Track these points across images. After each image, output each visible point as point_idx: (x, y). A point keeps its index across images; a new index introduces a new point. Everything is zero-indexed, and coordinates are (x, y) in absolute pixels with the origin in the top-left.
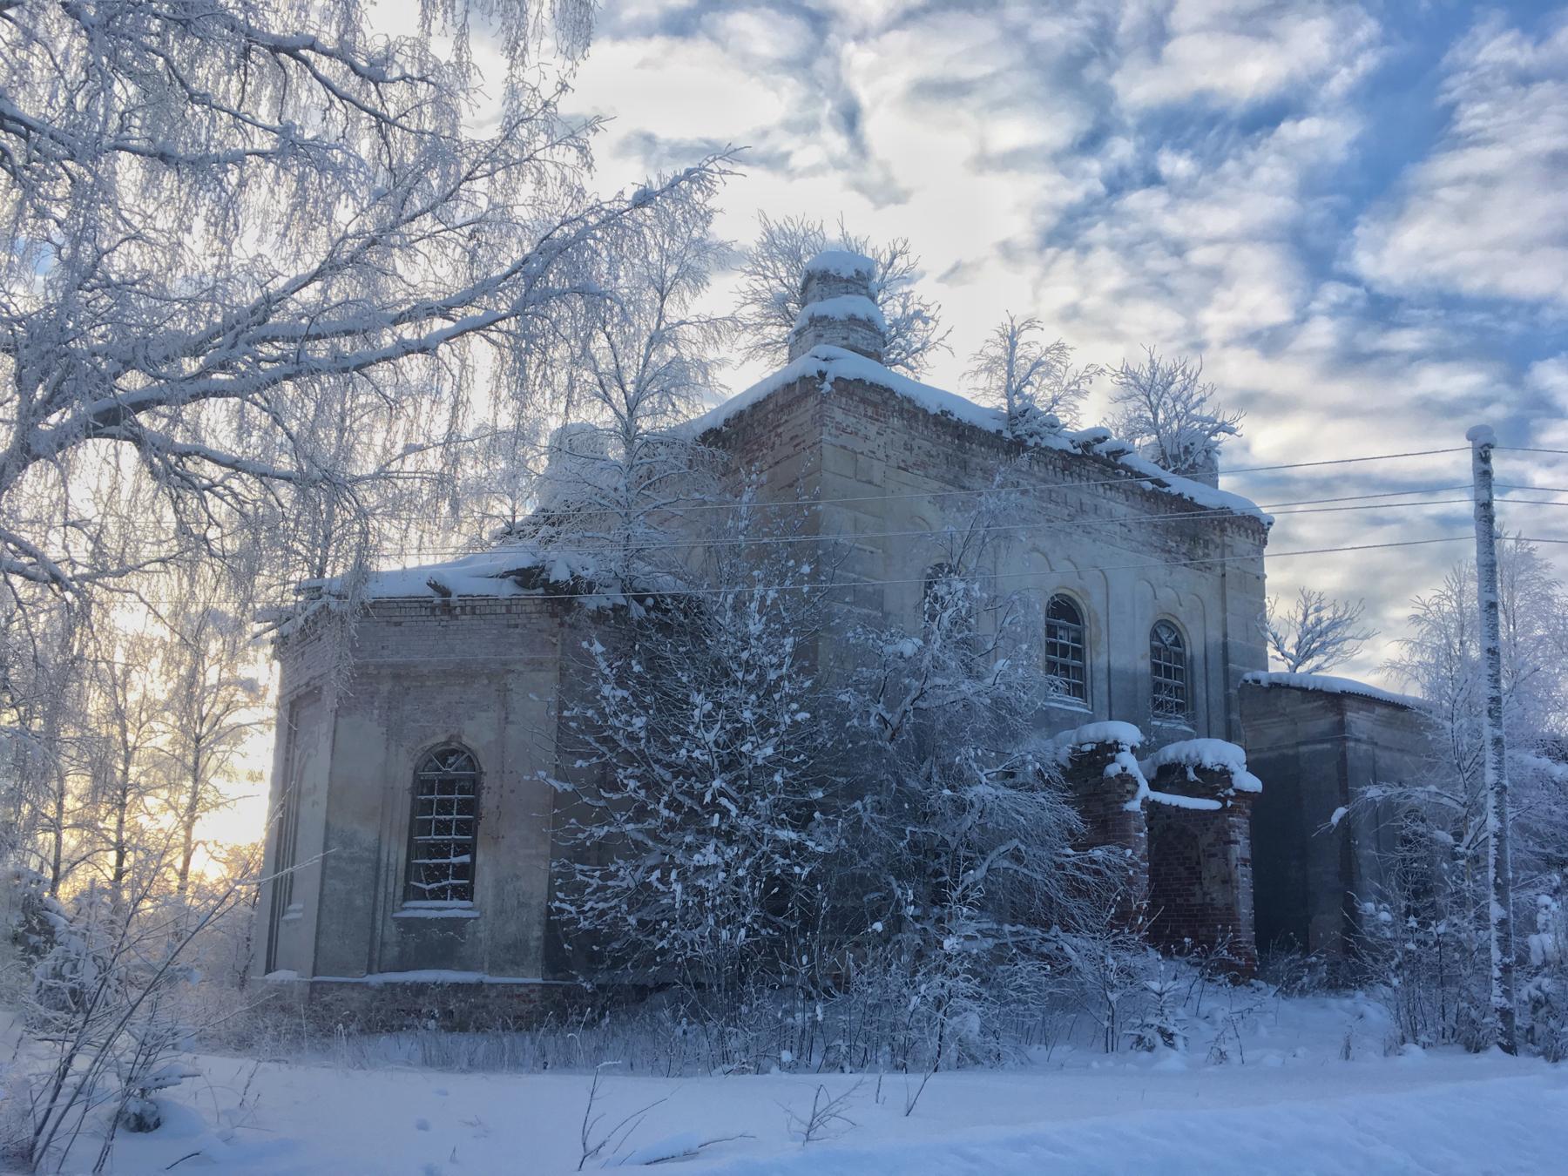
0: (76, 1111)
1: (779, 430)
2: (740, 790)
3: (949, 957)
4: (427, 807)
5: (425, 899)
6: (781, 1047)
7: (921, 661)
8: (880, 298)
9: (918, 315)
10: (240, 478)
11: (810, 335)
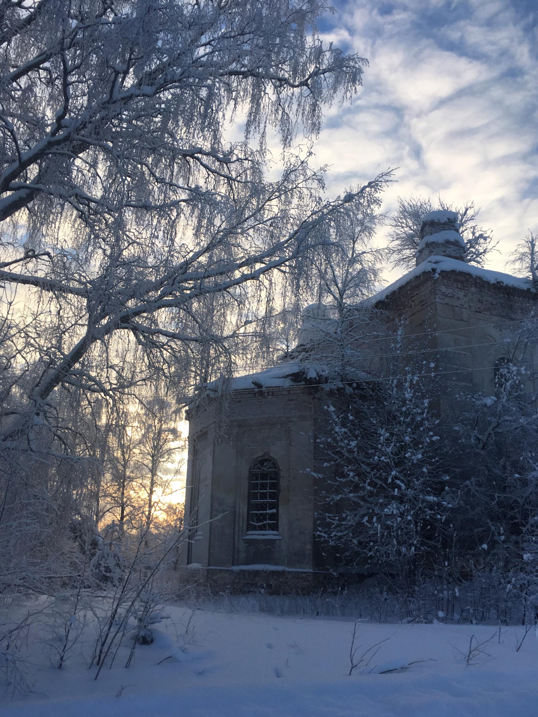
0: (120, 634)
1: (414, 299)
2: (405, 475)
3: (527, 564)
4: (255, 486)
5: (256, 530)
6: (438, 609)
7: (497, 409)
8: (460, 230)
9: (481, 236)
10: (174, 341)
11: (426, 252)
